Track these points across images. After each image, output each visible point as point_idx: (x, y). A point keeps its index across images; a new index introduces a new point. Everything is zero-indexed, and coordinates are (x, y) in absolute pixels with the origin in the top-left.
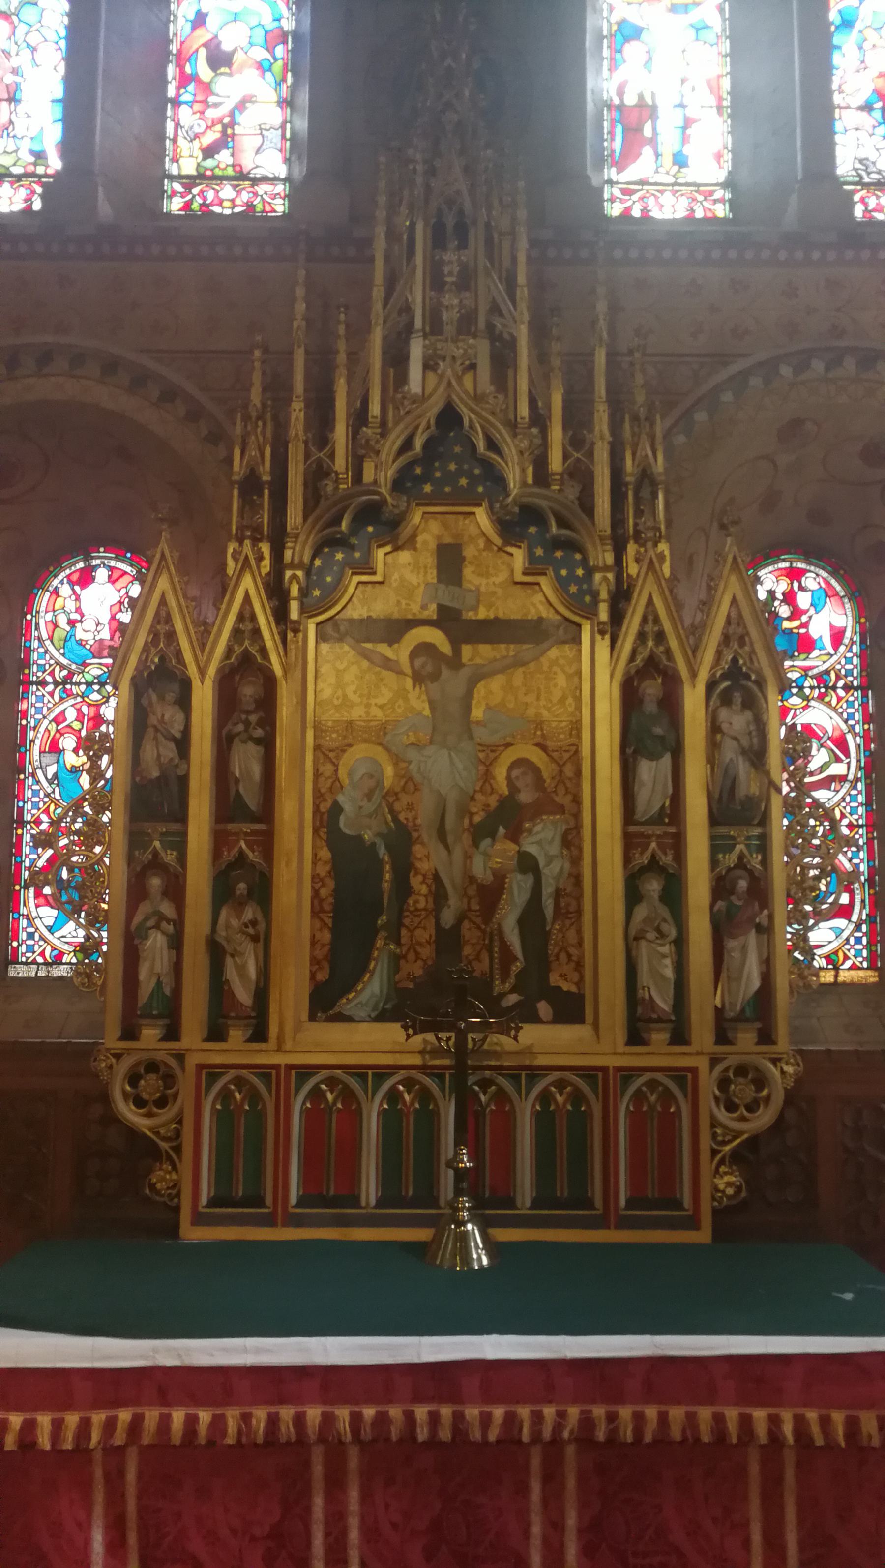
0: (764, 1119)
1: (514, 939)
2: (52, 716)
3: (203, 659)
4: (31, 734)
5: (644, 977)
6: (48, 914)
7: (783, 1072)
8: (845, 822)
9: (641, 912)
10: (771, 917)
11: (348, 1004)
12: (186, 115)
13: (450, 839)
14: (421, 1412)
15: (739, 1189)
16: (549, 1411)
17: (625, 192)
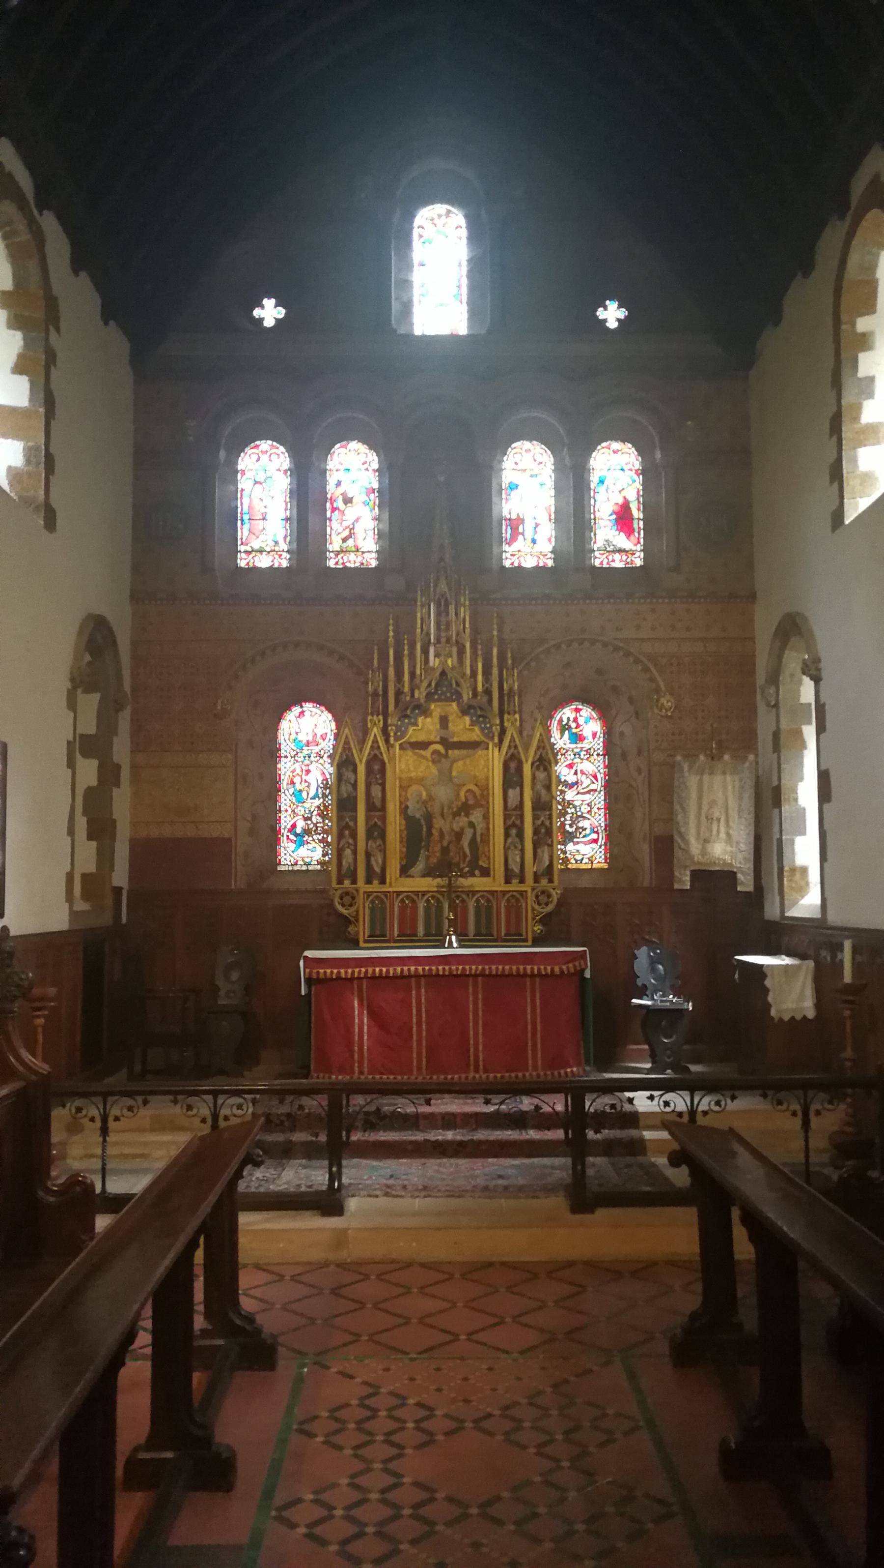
0: (550, 908)
1: (467, 851)
2: (291, 770)
3: (361, 756)
4: (282, 777)
5: (510, 861)
6: (292, 846)
7: (556, 893)
8: (596, 807)
9: (509, 840)
10: (552, 842)
11: (413, 871)
12: (335, 524)
13: (445, 817)
14: (440, 968)
15: (542, 931)
16: (474, 967)
17: (512, 555)
